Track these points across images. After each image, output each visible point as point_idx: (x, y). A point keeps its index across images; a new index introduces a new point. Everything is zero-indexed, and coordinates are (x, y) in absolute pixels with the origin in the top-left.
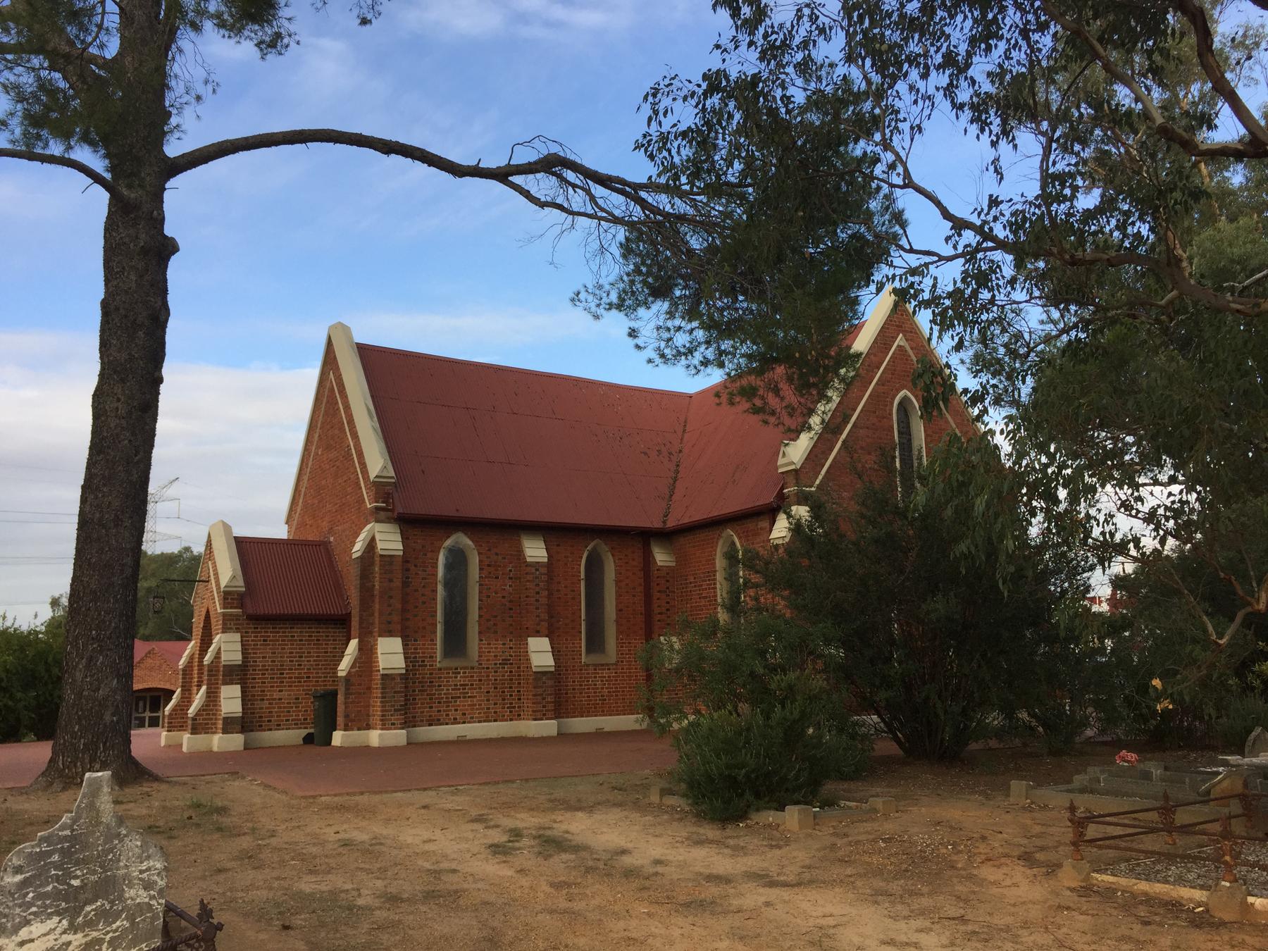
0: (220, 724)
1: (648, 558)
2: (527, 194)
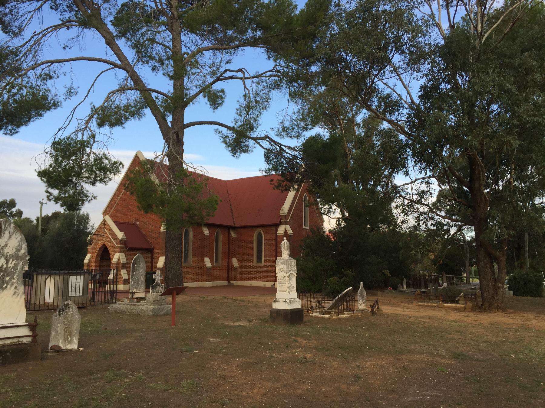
0: (122, 281)
1: (229, 234)
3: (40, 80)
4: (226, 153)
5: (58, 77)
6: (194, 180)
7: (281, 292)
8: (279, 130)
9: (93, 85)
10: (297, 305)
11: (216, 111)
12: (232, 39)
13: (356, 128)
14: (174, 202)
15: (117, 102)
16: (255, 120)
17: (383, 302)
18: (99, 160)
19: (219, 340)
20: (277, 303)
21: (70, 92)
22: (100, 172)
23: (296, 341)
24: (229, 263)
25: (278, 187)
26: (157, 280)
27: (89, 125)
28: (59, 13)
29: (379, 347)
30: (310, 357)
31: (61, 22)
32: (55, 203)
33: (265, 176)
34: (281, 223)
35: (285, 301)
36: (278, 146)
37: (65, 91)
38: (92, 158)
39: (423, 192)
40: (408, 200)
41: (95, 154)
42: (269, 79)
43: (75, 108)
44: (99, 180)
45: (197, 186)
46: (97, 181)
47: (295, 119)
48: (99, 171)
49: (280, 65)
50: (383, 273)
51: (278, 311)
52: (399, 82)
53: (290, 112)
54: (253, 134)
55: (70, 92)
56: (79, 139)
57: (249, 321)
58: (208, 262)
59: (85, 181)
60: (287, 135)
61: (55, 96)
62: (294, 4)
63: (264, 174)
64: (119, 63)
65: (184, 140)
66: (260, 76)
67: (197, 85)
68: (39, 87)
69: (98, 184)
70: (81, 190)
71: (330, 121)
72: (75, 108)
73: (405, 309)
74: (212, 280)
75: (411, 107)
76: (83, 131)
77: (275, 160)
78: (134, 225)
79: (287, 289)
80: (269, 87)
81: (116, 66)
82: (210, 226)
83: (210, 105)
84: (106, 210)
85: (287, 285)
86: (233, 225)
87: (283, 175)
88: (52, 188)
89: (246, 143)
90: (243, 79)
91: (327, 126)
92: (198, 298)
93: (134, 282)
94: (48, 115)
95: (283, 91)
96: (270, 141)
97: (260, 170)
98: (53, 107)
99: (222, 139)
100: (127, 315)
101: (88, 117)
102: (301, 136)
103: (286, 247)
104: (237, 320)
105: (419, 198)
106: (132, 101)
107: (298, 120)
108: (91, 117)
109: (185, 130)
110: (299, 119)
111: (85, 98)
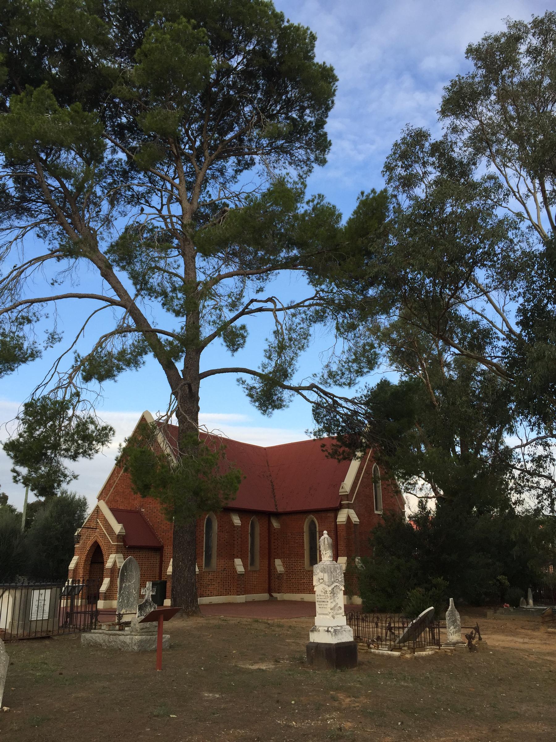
1: (270, 524)
2: (305, 397)
3: (16, 324)
4: (253, 410)
5: (38, 320)
6: (207, 448)
7: (322, 616)
8: (323, 376)
9: (83, 329)
10: (347, 636)
11: (236, 354)
12: (263, 261)
13: (445, 369)
14: (178, 481)
15: (109, 348)
16: (290, 364)
17: (494, 628)
18: (82, 426)
19: (217, 696)
20: (316, 633)
21: (53, 338)
22: (84, 442)
23: (334, 699)
24: (271, 567)
25: (334, 454)
26: (146, 596)
27: (74, 381)
28: (47, 242)
29: (468, 709)
30: (350, 728)
31: (50, 252)
32: (23, 485)
33: (314, 440)
34: (341, 507)
35: (328, 631)
36: (330, 398)
37: (46, 336)
38: (74, 423)
39: (540, 457)
40: (518, 469)
41: (79, 417)
42: (309, 309)
43: (60, 358)
44: (82, 453)
45: (210, 457)
46: (79, 453)
47: (345, 360)
48: (81, 440)
49: (323, 291)
50: (498, 580)
51: (318, 646)
52: (489, 305)
53: (338, 352)
54: (294, 382)
55: (52, 338)
56: (58, 399)
57: (277, 661)
58: (239, 565)
59: (63, 454)
60: (335, 382)
61: (33, 344)
62: (337, 213)
63: (313, 437)
64: (117, 298)
65: (200, 394)
66: (298, 305)
67: (210, 321)
68: (14, 333)
69: (80, 458)
70: (57, 467)
71: (408, 361)
72: (60, 358)
73: (526, 640)
74: (246, 592)
75: (508, 337)
76: (66, 388)
77: (328, 417)
78: (138, 513)
79: (330, 611)
80: (310, 319)
81: (113, 303)
82: (242, 512)
83: (227, 346)
84: (102, 492)
85: (330, 605)
86: (275, 510)
87: (339, 438)
88: (21, 466)
89: (279, 395)
90: (274, 311)
91: (405, 368)
92: (215, 622)
93: (123, 599)
94: (23, 369)
95: (328, 324)
96: (319, 392)
97: (306, 432)
98: (30, 359)
99: (247, 392)
100: (104, 649)
101: (71, 370)
102: (355, 384)
103: (327, 546)
104: (261, 659)
105: (534, 467)
106: (128, 347)
107: (349, 361)
108: (76, 369)
109: (202, 381)
110: (350, 360)
111: (73, 345)
